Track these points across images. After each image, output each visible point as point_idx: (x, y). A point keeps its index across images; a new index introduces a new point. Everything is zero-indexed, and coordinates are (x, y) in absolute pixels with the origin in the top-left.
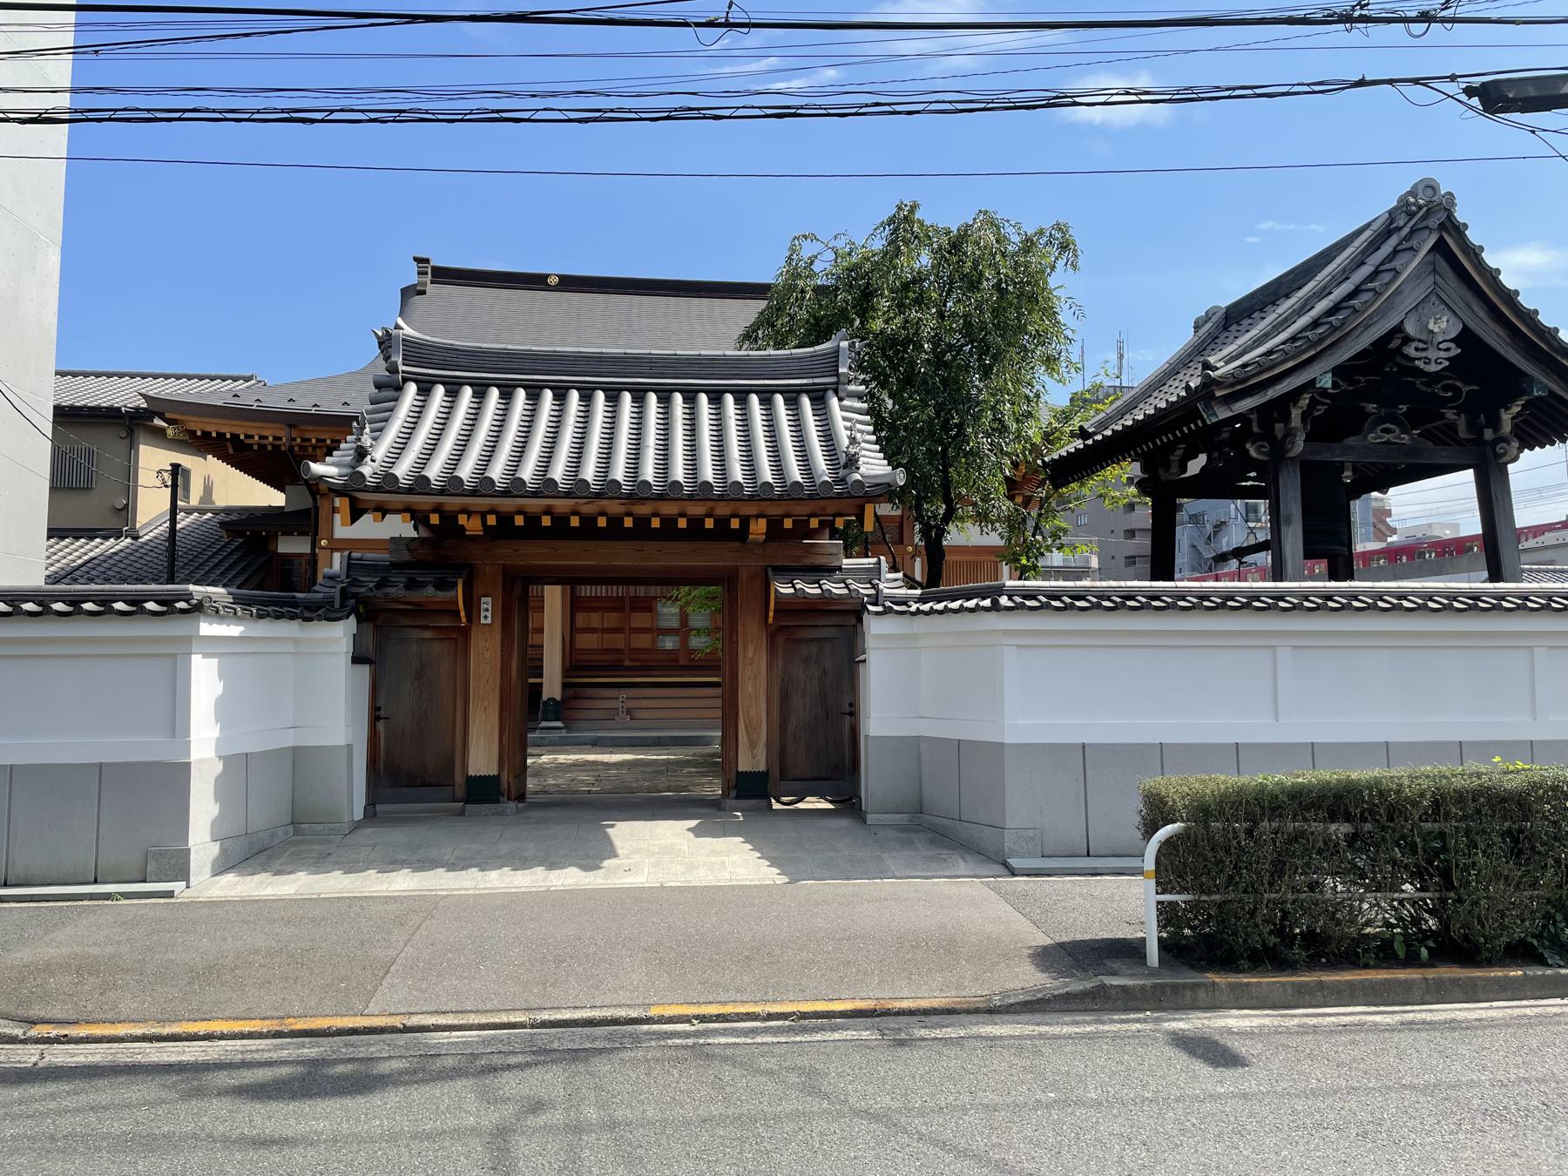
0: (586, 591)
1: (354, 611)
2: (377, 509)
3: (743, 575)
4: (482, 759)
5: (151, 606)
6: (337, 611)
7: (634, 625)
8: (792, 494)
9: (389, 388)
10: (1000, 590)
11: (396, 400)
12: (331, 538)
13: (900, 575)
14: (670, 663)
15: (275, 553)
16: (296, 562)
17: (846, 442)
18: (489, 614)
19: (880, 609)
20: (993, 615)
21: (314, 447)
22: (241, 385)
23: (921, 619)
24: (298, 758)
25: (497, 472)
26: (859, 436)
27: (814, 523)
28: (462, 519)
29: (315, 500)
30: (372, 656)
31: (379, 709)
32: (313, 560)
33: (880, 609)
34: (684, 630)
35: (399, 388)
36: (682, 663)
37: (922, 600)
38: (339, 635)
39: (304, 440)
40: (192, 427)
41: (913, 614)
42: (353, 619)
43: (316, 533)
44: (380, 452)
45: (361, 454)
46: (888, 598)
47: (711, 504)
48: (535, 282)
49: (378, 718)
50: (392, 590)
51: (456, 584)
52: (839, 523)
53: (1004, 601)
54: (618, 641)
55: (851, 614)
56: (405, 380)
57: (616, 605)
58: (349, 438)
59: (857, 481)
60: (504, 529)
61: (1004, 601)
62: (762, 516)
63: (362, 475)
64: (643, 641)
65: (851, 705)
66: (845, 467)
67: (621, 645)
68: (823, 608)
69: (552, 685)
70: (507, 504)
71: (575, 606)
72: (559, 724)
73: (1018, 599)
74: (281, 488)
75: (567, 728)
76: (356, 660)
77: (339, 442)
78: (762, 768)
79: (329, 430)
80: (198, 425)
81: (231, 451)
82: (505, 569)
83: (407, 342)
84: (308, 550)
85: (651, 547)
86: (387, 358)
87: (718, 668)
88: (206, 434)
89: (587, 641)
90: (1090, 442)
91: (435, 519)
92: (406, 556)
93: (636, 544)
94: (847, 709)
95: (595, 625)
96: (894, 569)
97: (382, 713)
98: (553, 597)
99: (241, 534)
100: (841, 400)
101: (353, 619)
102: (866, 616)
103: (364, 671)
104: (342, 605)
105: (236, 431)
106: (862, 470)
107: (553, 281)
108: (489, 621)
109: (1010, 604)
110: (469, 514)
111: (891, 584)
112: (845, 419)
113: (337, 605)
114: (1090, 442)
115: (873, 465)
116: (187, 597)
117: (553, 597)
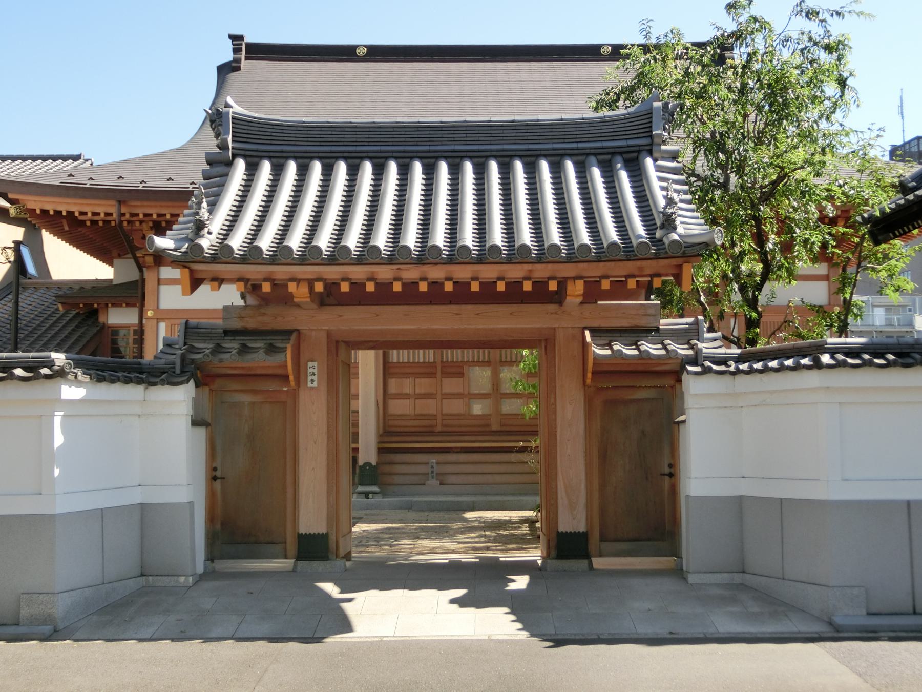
0: (395, 356)
1: (193, 376)
2: (214, 279)
3: (560, 336)
4: (311, 519)
5: (19, 372)
6: (179, 376)
7: (447, 390)
8: (604, 253)
9: (218, 166)
10: (823, 348)
11: (227, 175)
12: (157, 309)
13: (719, 334)
14: (482, 428)
15: (104, 327)
16: (122, 332)
17: (662, 203)
18: (315, 378)
19: (698, 369)
20: (814, 375)
21: (141, 222)
22: (70, 165)
23: (740, 378)
24: (145, 513)
25: (266, 242)
26: (676, 197)
27: (632, 284)
28: (292, 287)
29: (141, 271)
30: (208, 418)
31: (215, 469)
32: (140, 332)
33: (698, 369)
34: (497, 393)
35: (230, 164)
36: (494, 428)
37: (739, 359)
38: (179, 399)
39: (132, 215)
40: (31, 205)
41: (733, 374)
42: (192, 383)
43: (142, 305)
44: (216, 224)
45: (200, 226)
46: (707, 358)
47: (530, 267)
48: (345, 53)
49: (215, 478)
50: (227, 356)
51: (284, 350)
52: (657, 283)
53: (826, 359)
54: (430, 407)
55: (672, 374)
56: (235, 156)
57: (428, 370)
58: (186, 212)
59: (675, 241)
60: (329, 296)
61: (826, 359)
62: (581, 278)
63: (200, 248)
64: (455, 407)
65: (671, 466)
66: (663, 227)
67: (433, 411)
68: (644, 369)
69: (368, 454)
70: (332, 272)
71: (387, 370)
72: (375, 489)
73: (840, 357)
74: (110, 262)
75: (384, 494)
76: (195, 423)
77: (178, 215)
78: (582, 528)
79: (166, 206)
80: (36, 203)
81: (66, 228)
82: (329, 334)
83: (238, 121)
84: (135, 321)
85: (468, 310)
86: (217, 136)
87: (535, 433)
88: (45, 212)
89: (398, 407)
90: (911, 197)
91: (266, 287)
92: (236, 324)
93: (454, 308)
94: (667, 470)
95: (407, 390)
96: (711, 329)
97: (218, 474)
98: (367, 362)
99: (77, 306)
100: (655, 160)
101: (192, 383)
102: (685, 377)
103: (202, 432)
104: (183, 372)
105: (71, 208)
106: (680, 229)
107: (361, 52)
108: (315, 385)
109: (832, 362)
110: (298, 281)
111: (709, 346)
112: (661, 179)
113: (178, 371)
114: (911, 197)
115: (689, 225)
116: (50, 364)
117: (367, 362)
